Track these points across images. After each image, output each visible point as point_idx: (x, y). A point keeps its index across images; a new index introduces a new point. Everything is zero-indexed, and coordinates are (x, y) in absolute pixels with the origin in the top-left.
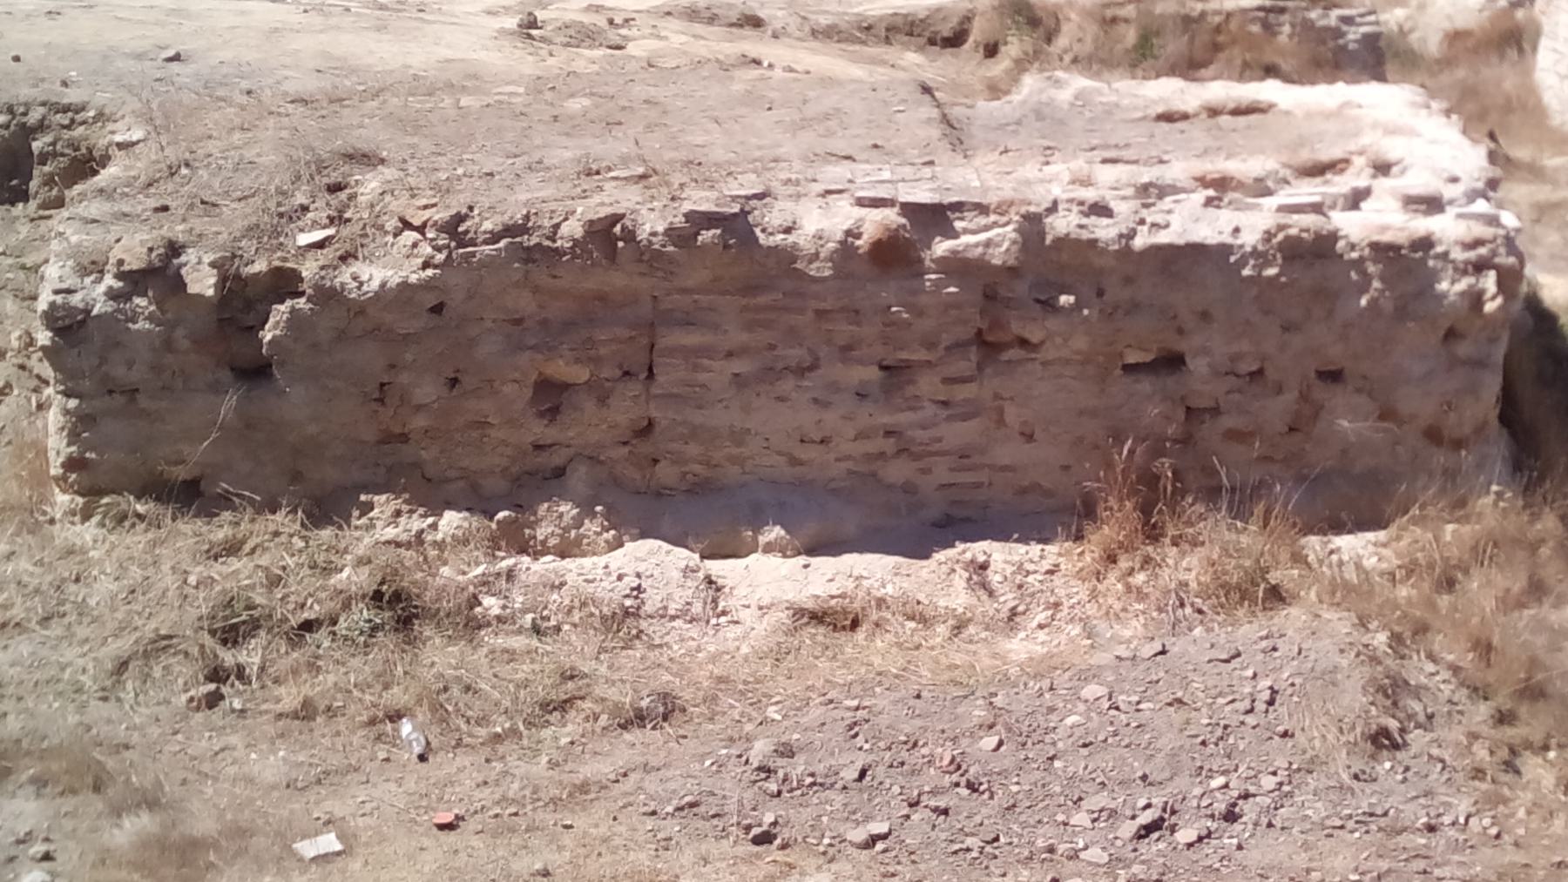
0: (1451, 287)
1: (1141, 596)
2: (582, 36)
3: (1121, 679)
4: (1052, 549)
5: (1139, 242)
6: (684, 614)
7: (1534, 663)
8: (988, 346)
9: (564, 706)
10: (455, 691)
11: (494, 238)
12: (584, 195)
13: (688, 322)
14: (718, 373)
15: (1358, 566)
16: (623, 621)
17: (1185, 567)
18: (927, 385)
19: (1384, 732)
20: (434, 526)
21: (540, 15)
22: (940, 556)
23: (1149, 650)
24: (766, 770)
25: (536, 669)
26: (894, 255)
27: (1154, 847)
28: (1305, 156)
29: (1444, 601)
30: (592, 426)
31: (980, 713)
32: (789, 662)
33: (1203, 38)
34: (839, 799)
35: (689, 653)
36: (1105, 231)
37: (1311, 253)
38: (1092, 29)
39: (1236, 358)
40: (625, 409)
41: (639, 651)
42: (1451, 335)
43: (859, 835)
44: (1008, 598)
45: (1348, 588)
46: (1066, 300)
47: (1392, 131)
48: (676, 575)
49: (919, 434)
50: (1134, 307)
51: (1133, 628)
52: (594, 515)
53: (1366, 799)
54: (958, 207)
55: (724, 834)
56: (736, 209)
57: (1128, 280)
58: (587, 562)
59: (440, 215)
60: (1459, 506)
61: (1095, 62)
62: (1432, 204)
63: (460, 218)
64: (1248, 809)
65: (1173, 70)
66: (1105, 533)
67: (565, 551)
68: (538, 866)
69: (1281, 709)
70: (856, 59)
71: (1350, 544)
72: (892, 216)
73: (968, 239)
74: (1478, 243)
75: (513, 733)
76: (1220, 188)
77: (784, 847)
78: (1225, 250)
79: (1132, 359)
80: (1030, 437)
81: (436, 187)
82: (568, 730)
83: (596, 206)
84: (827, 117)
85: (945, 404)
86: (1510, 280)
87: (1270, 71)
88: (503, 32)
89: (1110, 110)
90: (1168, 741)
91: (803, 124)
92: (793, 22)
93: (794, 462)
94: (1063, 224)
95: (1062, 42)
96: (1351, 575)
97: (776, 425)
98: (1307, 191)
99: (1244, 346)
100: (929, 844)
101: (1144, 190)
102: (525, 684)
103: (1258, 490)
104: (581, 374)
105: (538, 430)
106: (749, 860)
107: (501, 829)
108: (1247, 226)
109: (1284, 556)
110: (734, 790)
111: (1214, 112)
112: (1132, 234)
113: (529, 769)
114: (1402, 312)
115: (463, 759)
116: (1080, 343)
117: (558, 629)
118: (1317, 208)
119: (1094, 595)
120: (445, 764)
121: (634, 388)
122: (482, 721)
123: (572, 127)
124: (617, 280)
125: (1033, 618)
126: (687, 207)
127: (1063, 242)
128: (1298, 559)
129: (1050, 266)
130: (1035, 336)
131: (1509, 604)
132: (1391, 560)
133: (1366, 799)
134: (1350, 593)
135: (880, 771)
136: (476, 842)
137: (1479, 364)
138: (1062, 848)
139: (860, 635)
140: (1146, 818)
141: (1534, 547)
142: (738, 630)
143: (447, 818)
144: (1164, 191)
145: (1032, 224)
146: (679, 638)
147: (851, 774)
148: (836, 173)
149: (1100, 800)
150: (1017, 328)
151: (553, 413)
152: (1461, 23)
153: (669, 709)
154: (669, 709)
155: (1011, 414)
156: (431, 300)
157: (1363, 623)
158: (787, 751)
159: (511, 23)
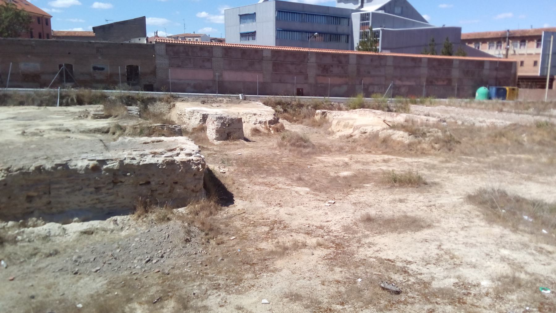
0: (194, 167)
1: (145, 222)
2: (34, 134)
3: (142, 237)
4: (129, 216)
5: (141, 164)
6: (59, 235)
7: (211, 225)
8: (115, 183)
9: (35, 254)
10: (13, 255)
11: (16, 171)
12: (35, 162)
13: (57, 183)
14: (63, 192)
15: (182, 213)
16: (46, 238)
17: (152, 216)
18: (104, 190)
19: (187, 239)
20: (7, 225)
21: (26, 131)
22: (108, 220)
23: (147, 231)
24: (76, 261)
25: (29, 247)
26: (96, 169)
27: (149, 264)
28: (169, 148)
29: (196, 217)
30: (38, 203)
31: (116, 246)
32: (80, 241)
33: (151, 130)
34: (90, 264)
35: (59, 242)
36: (135, 162)
37: (171, 164)
38: (132, 129)
39: (159, 181)
40: (45, 199)
41: (50, 243)
42: (195, 175)
43: (94, 270)
44: (121, 225)
45: (180, 217)
46: (128, 174)
47: (183, 144)
48: (57, 228)
49: (103, 199)
50: (141, 175)
51: (144, 228)
52: (39, 219)
53: (185, 251)
54: (108, 160)
55: (68, 273)
56: (65, 163)
57: (139, 170)
58: (39, 228)
59: (5, 168)
60: (198, 202)
61: (133, 134)
62: (190, 155)
63: (9, 168)
64: (165, 255)
65: (146, 136)
66: (138, 212)
67: (35, 226)
68: (31, 284)
69: (170, 238)
70: (88, 136)
71: (180, 210)
72: (95, 162)
73: (110, 165)
74: (198, 160)
75: (25, 261)
76: (155, 154)
77: (80, 274)
78: (156, 164)
79: (141, 183)
80: (123, 198)
81: (4, 163)
82: (36, 259)
83: (37, 164)
84: (82, 146)
85: (107, 193)
86: (203, 166)
87: (163, 135)
88: (18, 134)
89: (135, 142)
90: (150, 246)
91: (78, 147)
92: (76, 130)
93: (79, 206)
94: (127, 161)
95: (127, 132)
96: (181, 215)
97: (75, 200)
98: (169, 154)
99: (161, 179)
100: (108, 270)
101: (141, 155)
102: (27, 251)
103: (164, 203)
104: (35, 194)
105: (28, 205)
106: (73, 278)
107: (23, 279)
108: (160, 160)
109: (170, 213)
110: (70, 266)
111: (153, 142)
112: (140, 162)
113: (28, 267)
114: (187, 172)
115: (15, 267)
116: (132, 181)
117: (33, 241)
118: (171, 156)
119: (137, 223)
120: (11, 268)
121: (46, 196)
122: (19, 259)
123: (32, 150)
124: (42, 177)
125: (127, 228)
126: (55, 163)
127: (127, 164)
128: (172, 213)
129: (125, 168)
130: (123, 180)
131: (207, 216)
132: (188, 211)
133: (185, 251)
134: (181, 217)
135: (98, 258)
136: (18, 282)
137: (199, 179)
138: (132, 267)
139: (93, 235)
140: (147, 259)
141: (210, 207)
142: (70, 237)
143: (11, 278)
144: (145, 155)
145: (121, 162)
146: (58, 240)
147: (92, 260)
148: (84, 156)
149: (139, 258)
150: (120, 179)
151: (30, 202)
152: (194, 127)
153: (56, 253)
154: (56, 253)
155: (120, 194)
156: (3, 183)
157: (183, 222)
158: (80, 257)
159: (20, 132)
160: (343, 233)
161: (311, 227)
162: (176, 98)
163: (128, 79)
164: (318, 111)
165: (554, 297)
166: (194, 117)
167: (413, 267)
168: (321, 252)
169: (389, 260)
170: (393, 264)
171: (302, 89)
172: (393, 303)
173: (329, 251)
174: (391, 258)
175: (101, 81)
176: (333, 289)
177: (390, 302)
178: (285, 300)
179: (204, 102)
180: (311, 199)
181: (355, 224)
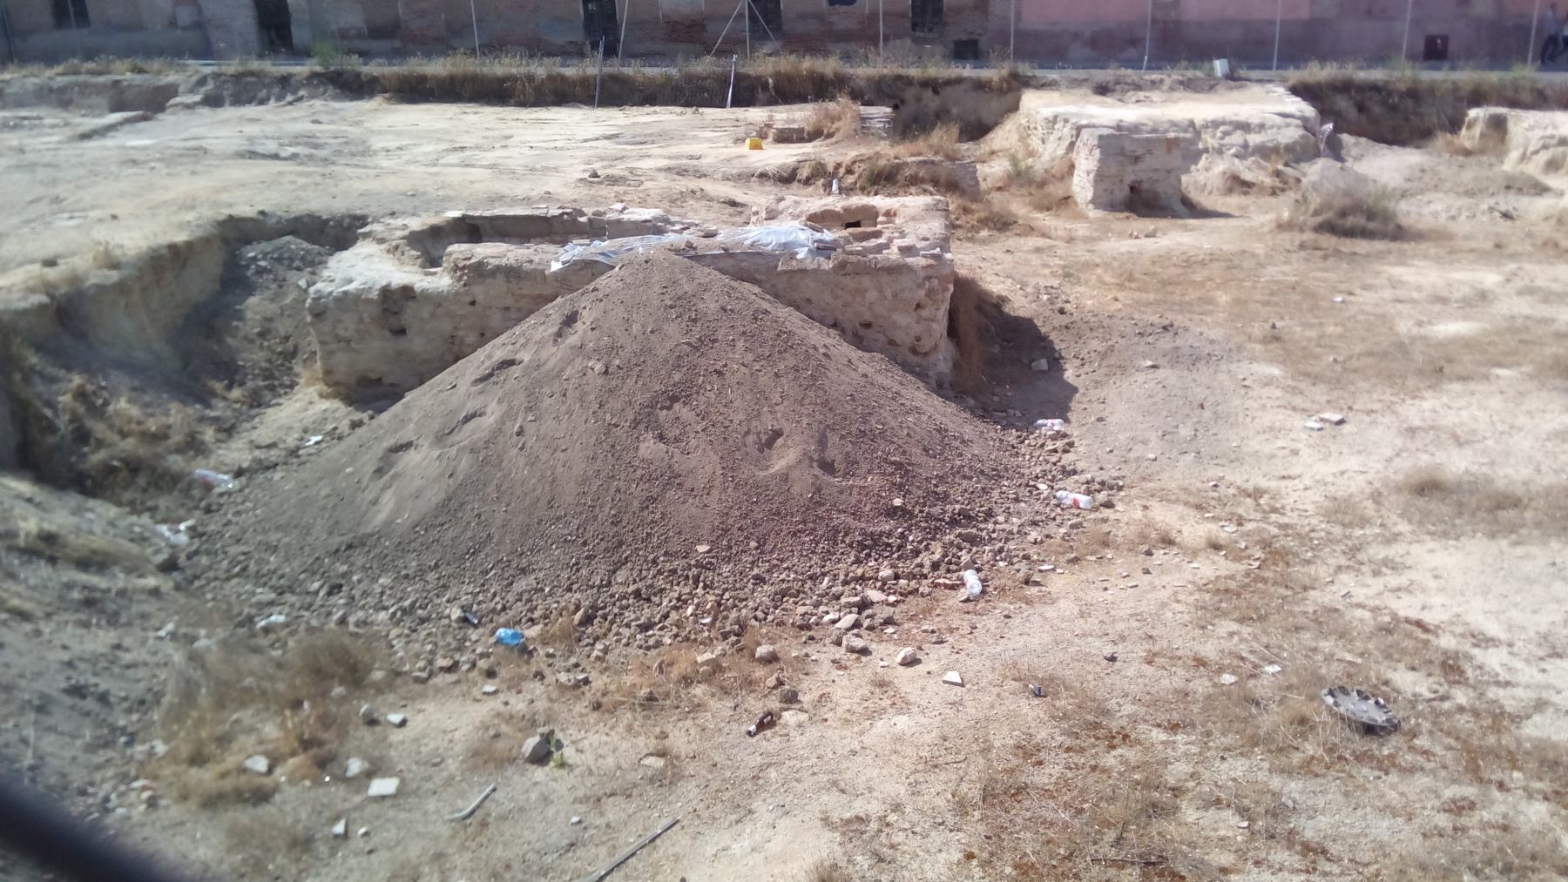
160: (1314, 521)
161: (1222, 489)
162: (1024, 82)
163: (914, 26)
164: (1473, 113)
165: (1023, 868)
166: (1057, 134)
167: (1493, 659)
168: (1211, 568)
169: (1419, 624)
170: (1424, 636)
171: (1445, 39)
172: (1340, 758)
173: (1239, 568)
174: (1428, 618)
175: (845, 37)
176: (1173, 680)
177: (1330, 751)
178: (1012, 685)
179: (1102, 90)
180: (1269, 403)
181: (1376, 497)
